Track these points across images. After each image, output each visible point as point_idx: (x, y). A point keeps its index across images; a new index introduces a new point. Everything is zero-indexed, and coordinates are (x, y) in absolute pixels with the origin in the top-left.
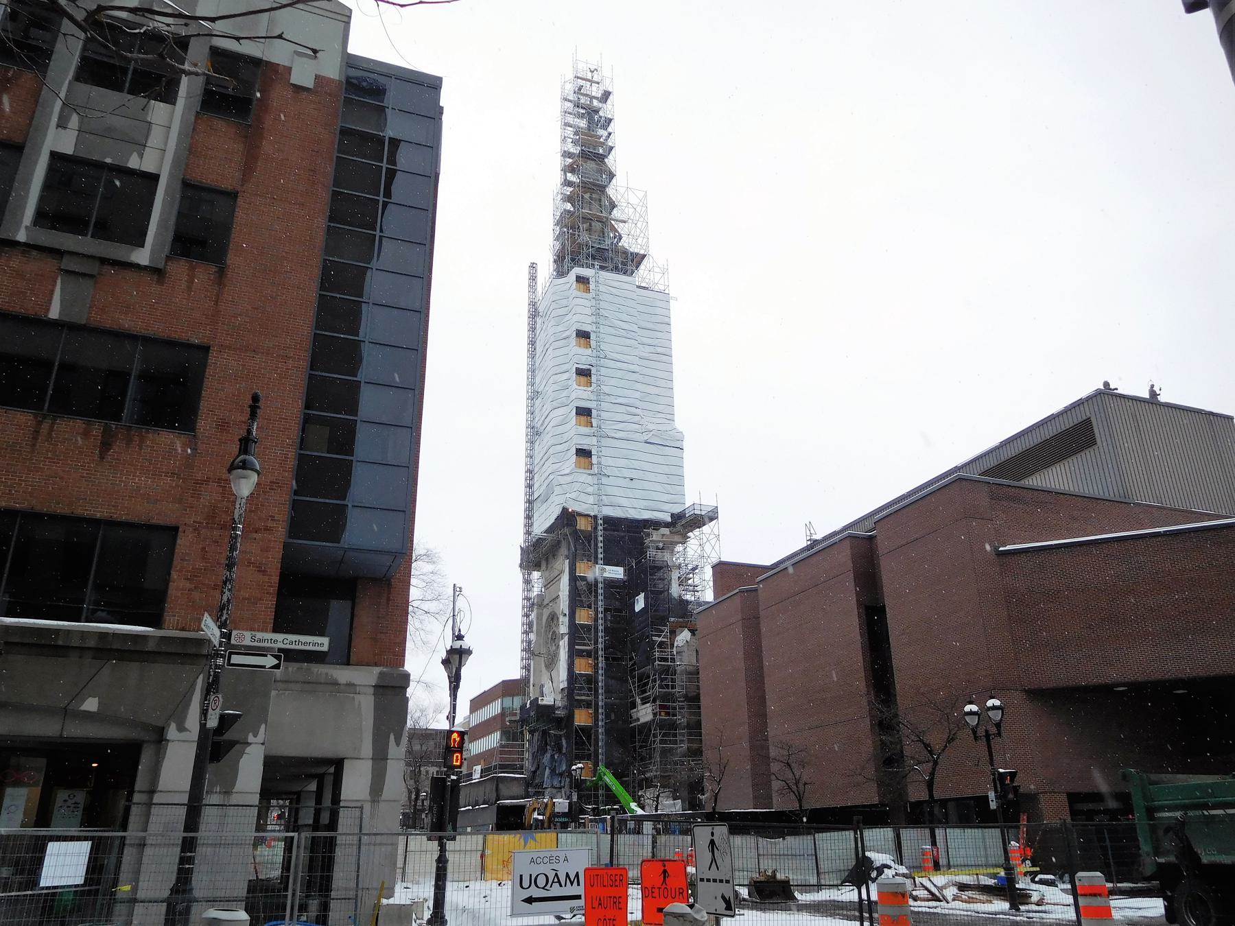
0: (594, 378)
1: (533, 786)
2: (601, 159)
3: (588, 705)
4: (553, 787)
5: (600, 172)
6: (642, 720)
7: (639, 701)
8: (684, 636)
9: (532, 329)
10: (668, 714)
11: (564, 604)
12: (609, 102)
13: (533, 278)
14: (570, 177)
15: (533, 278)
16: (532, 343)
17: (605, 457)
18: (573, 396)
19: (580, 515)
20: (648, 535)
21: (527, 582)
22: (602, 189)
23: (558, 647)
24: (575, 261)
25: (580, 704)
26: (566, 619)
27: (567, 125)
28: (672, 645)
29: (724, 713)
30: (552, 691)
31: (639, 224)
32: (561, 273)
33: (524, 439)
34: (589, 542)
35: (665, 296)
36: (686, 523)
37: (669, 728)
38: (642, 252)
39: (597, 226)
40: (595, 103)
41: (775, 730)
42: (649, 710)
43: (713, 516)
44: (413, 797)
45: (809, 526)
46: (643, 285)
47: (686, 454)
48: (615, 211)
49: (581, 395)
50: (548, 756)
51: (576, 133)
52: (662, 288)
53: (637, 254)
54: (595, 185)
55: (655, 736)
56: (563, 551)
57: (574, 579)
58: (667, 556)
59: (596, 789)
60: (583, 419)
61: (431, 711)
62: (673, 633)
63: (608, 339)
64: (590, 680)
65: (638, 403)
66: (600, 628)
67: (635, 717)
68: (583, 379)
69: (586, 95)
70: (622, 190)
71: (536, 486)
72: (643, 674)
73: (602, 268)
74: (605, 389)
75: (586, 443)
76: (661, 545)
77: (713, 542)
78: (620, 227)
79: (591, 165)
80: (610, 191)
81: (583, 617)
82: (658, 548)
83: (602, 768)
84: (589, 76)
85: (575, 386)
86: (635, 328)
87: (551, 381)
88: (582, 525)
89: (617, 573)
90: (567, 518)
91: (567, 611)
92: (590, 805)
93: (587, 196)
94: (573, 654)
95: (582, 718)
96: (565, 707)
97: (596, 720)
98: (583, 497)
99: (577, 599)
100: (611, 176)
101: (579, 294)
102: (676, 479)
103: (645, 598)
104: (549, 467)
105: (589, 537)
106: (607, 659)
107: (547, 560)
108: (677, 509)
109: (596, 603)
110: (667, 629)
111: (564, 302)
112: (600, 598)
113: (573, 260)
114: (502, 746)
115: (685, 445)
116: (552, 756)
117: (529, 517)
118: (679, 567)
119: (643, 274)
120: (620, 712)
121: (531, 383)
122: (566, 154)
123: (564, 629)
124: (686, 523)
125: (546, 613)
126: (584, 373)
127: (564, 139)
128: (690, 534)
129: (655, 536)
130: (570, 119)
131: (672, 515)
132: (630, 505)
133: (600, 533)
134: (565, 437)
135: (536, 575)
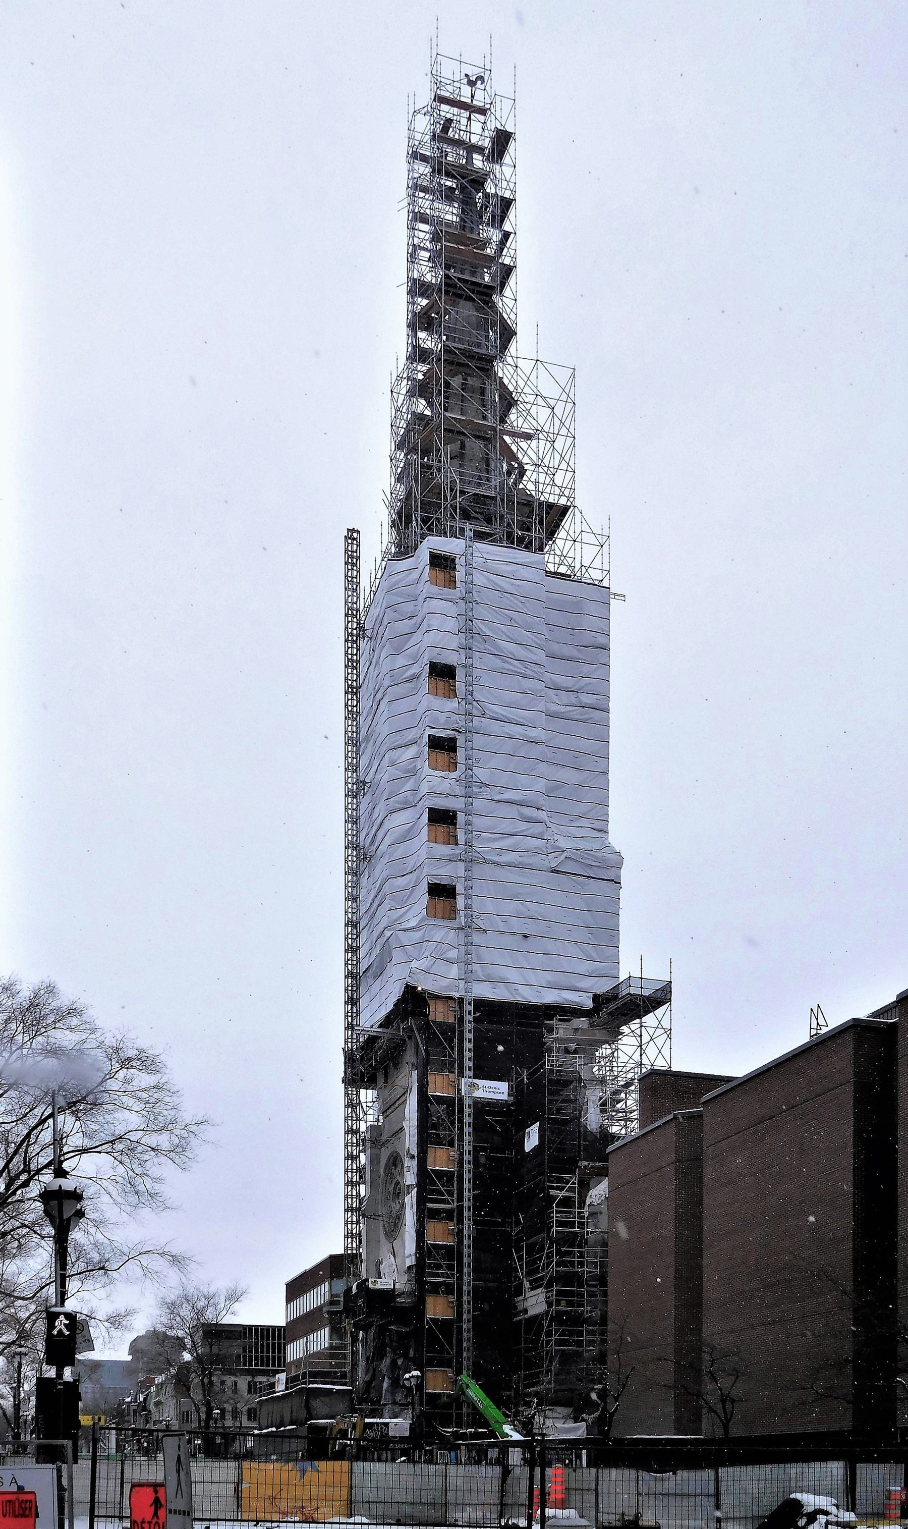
0: (461, 754)
1: (366, 1400)
2: (485, 296)
3: (449, 1289)
4: (394, 1403)
5: (484, 325)
6: (532, 1312)
7: (526, 1285)
8: (599, 1191)
9: (352, 663)
10: (570, 1303)
11: (410, 1141)
12: (507, 159)
13: (352, 560)
14: (427, 341)
15: (352, 560)
16: (353, 690)
17: (482, 900)
18: (424, 789)
19: (436, 997)
20: (551, 1030)
21: (352, 1105)
22: (485, 365)
23: (403, 1206)
24: (430, 526)
25: (435, 1289)
26: (415, 1163)
27: (419, 217)
28: (582, 1203)
29: (640, 1307)
30: (392, 1272)
31: (558, 445)
32: (403, 549)
33: (341, 868)
34: (450, 1041)
35: (602, 594)
36: (623, 1008)
37: (571, 1322)
38: (563, 501)
39: (475, 446)
40: (478, 161)
41: (713, 1329)
42: (542, 1298)
43: (660, 997)
44: (203, 1416)
45: (816, 1012)
46: (563, 570)
47: (625, 894)
48: (513, 416)
49: (438, 785)
50: (387, 1362)
51: (436, 238)
52: (596, 575)
53: (550, 506)
54: (471, 356)
55: (549, 1334)
56: (409, 1057)
57: (424, 1100)
58: (580, 1064)
59: (460, 1407)
60: (441, 829)
61: (223, 1298)
62: (584, 1186)
63: (486, 679)
64: (452, 1254)
65: (542, 801)
66: (466, 1176)
67: (520, 1308)
68: (442, 757)
69: (458, 143)
70: (526, 366)
71: (363, 952)
72: (533, 1245)
73: (480, 536)
74: (481, 773)
75: (445, 873)
76: (573, 1046)
77: (659, 1041)
78: (526, 452)
79: (466, 311)
80: (503, 371)
81: (440, 1160)
82: (567, 1051)
83: (464, 1378)
84: (465, 94)
85: (427, 770)
86: (540, 656)
87: (386, 761)
88: (438, 1013)
89: (496, 1090)
90: (413, 1001)
91: (414, 1151)
92: (438, 1431)
93: (456, 382)
94: (424, 1215)
95: (437, 1309)
96: (410, 1294)
97: (460, 1314)
98: (440, 967)
99: (428, 1133)
100: (508, 334)
101: (435, 589)
102: (605, 934)
103: (541, 1130)
104: (384, 917)
105: (451, 1032)
106: (476, 1222)
107: (386, 1069)
108: (603, 987)
109: (461, 1139)
110: (575, 1179)
111: (409, 608)
112: (467, 1129)
113: (425, 521)
114: (331, 1347)
115: (625, 875)
116: (394, 1362)
117: (352, 1001)
118: (602, 1082)
119: (569, 548)
120: (496, 1299)
121: (352, 767)
122: (417, 288)
123: (410, 1178)
124: (623, 1008)
125: (385, 1154)
126: (443, 746)
127: (413, 252)
128: (624, 1029)
129: (562, 1031)
130: (425, 203)
131: (596, 997)
132: (524, 984)
133: (468, 1026)
134: (411, 863)
135: (367, 1095)
